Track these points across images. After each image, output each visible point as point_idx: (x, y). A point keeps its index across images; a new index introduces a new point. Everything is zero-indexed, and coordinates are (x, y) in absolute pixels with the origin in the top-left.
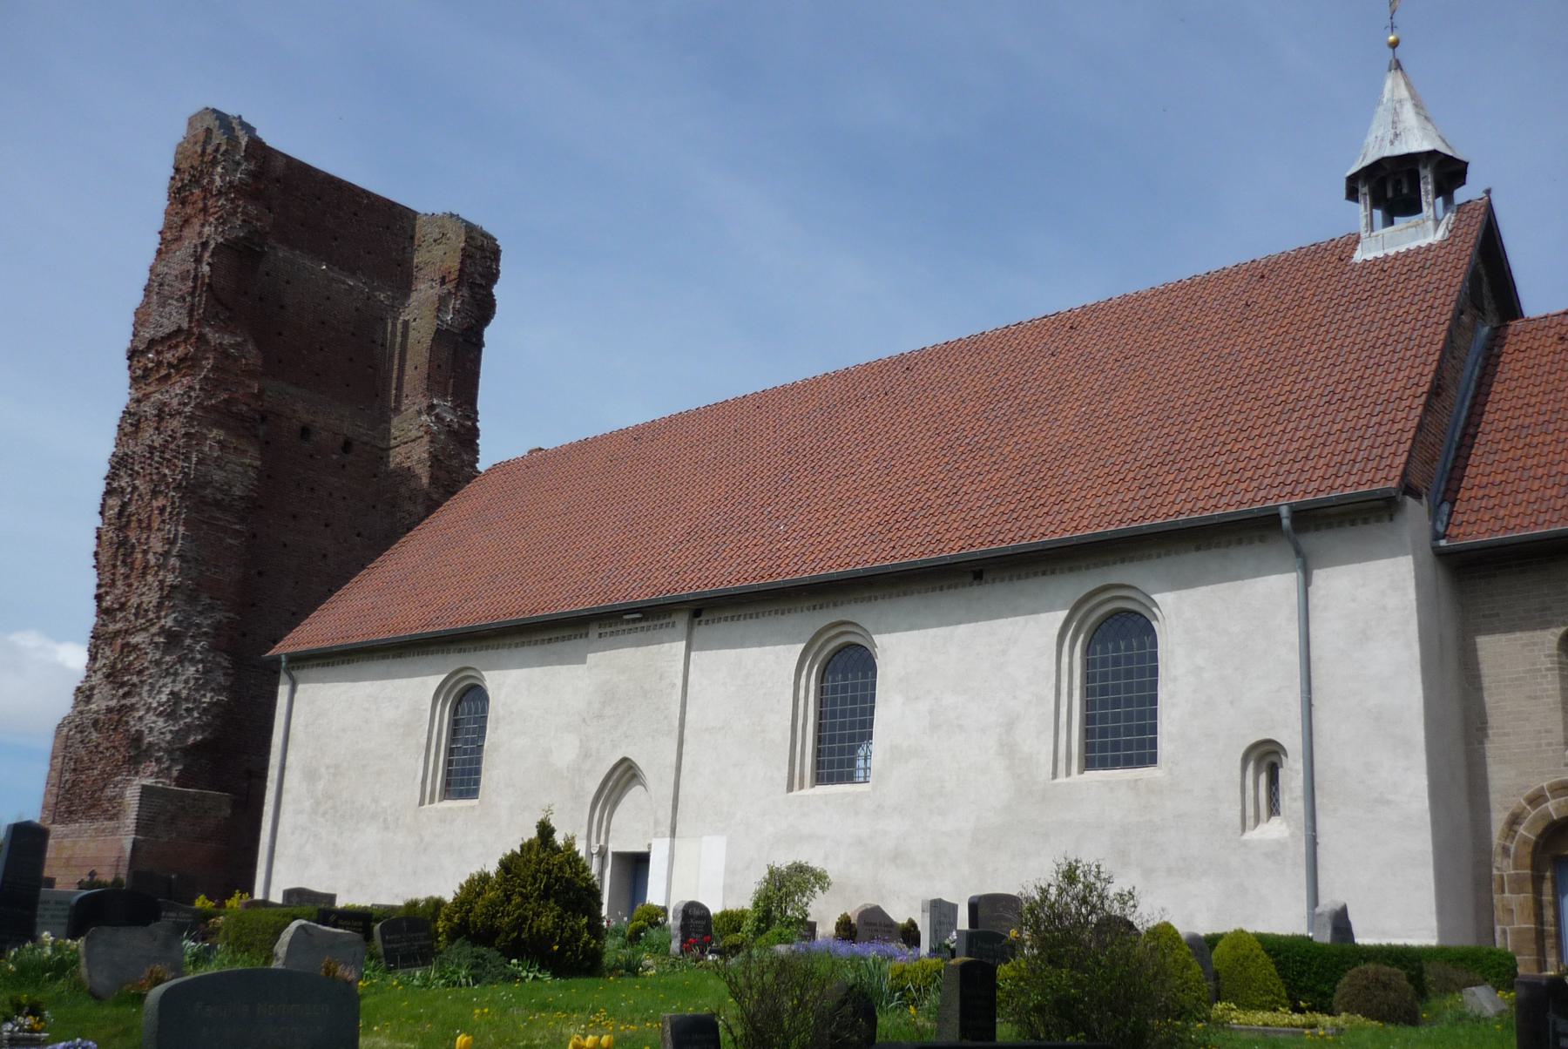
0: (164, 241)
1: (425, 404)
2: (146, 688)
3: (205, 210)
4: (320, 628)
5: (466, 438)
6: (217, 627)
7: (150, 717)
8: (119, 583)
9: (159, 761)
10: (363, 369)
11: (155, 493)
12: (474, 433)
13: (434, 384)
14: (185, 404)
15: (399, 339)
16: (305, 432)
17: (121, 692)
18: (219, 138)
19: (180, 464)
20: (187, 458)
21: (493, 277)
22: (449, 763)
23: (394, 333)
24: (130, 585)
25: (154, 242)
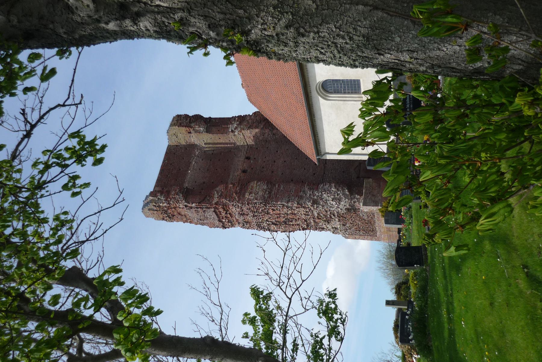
0: (186, 221)
1: (231, 134)
2: (331, 209)
3: (175, 208)
4: (309, 150)
5: (241, 119)
6: (310, 189)
7: (341, 206)
8: (298, 223)
9: (355, 202)
10: (221, 157)
11: (268, 213)
12: (240, 117)
13: (224, 131)
14: (238, 206)
15: (211, 146)
16: (244, 171)
17: (333, 217)
18: (151, 206)
19: (258, 205)
20: (256, 203)
21: (186, 116)
22: (349, 93)
23: (210, 147)
24: (299, 218)
25: (188, 224)
